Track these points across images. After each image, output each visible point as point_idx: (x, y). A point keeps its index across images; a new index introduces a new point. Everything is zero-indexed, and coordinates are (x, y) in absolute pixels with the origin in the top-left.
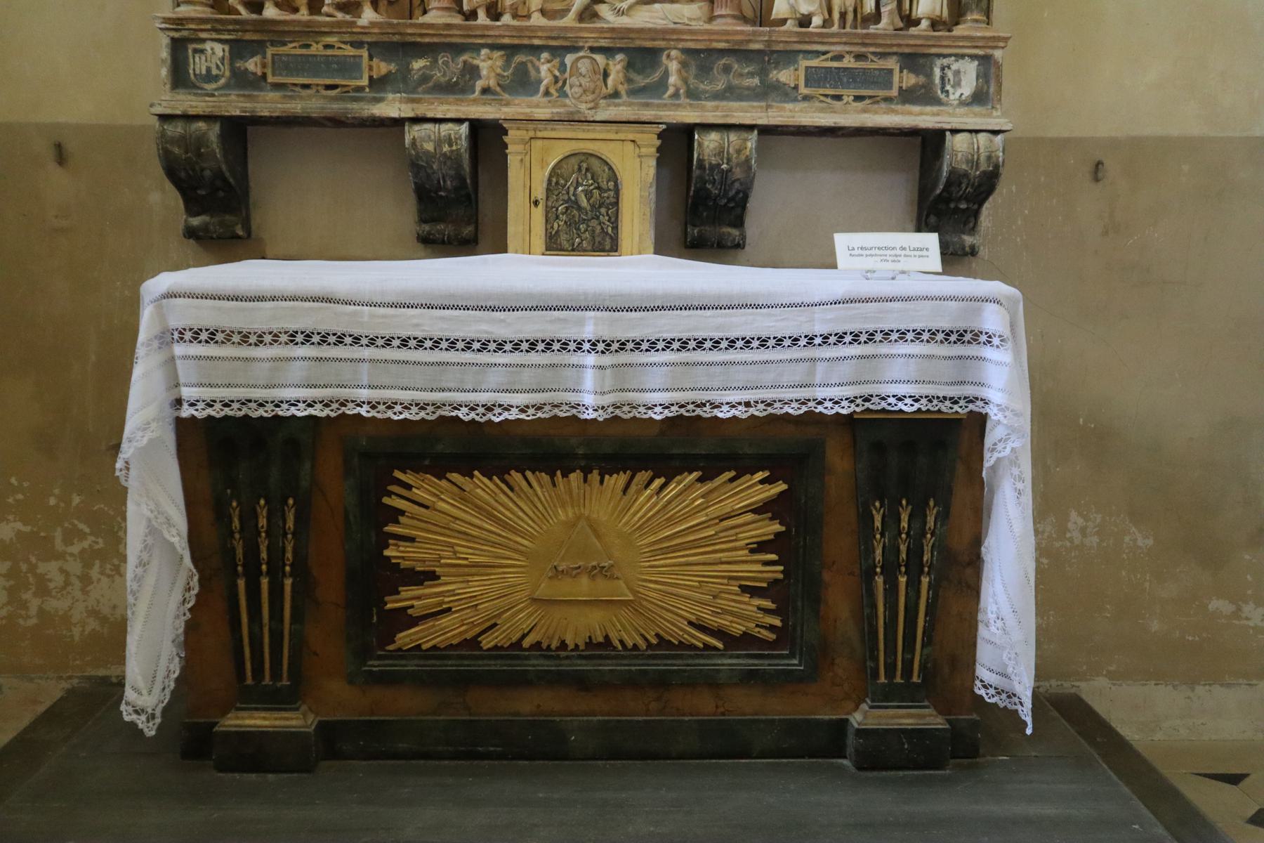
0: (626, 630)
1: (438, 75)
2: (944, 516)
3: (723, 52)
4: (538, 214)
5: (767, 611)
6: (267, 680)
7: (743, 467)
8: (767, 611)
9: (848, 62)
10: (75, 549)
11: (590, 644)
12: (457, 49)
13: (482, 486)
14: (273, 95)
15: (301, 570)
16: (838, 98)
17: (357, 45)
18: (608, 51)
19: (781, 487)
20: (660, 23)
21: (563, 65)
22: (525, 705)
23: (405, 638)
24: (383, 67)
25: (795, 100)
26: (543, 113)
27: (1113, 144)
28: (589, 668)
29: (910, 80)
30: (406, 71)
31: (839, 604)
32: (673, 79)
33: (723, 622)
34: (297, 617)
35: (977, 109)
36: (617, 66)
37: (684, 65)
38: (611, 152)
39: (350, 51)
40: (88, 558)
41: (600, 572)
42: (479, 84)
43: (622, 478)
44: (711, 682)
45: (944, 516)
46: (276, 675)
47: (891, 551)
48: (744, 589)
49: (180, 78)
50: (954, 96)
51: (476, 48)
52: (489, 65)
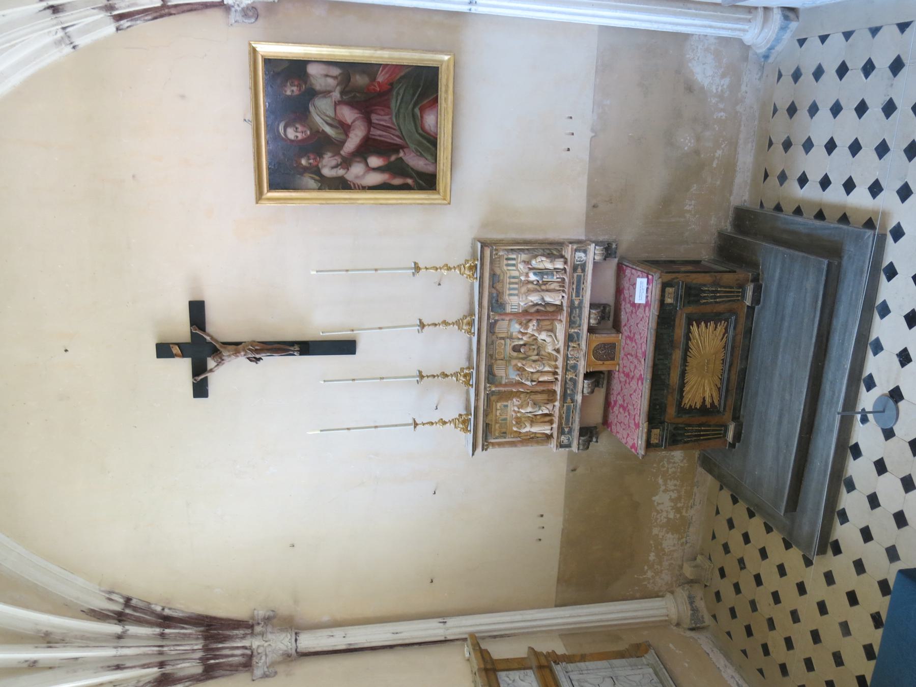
2: (705, 285)
4: (606, 362)
7: (689, 331)
9: (574, 286)
10: (666, 465)
12: (566, 383)
13: (687, 389)
15: (700, 425)
18: (568, 346)
22: (734, 377)
23: (716, 403)
24: (569, 400)
27: (588, 201)
29: (579, 270)
30: (570, 395)
31: (721, 308)
34: (709, 426)
36: (572, 344)
38: (594, 345)
40: (669, 463)
45: (705, 285)
47: (711, 297)
50: (584, 258)
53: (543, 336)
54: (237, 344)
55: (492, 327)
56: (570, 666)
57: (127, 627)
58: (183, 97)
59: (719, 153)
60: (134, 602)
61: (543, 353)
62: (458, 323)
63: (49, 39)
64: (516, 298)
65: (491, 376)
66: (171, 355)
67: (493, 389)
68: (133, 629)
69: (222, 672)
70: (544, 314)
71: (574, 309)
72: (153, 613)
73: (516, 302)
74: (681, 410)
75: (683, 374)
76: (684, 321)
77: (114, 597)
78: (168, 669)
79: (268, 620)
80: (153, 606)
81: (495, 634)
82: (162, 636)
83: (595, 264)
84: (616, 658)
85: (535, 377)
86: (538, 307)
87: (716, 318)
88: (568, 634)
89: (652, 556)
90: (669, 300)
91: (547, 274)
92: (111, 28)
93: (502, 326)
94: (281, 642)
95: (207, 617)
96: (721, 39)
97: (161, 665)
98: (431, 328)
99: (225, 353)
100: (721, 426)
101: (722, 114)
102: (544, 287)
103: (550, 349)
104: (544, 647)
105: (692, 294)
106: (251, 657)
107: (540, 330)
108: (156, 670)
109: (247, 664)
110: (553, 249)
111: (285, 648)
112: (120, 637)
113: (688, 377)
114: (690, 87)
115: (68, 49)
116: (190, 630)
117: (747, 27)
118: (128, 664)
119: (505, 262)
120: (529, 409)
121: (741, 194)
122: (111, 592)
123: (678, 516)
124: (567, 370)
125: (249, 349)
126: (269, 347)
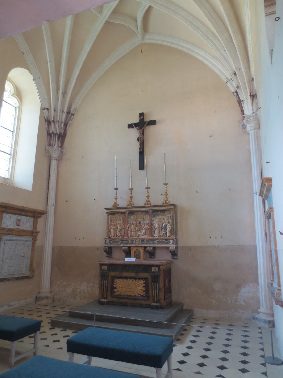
0: (133, 294)
1: (126, 243)
2: (159, 284)
3: (149, 240)
5: (144, 293)
6: (104, 297)
8: (144, 293)
9: (160, 240)
11: (130, 295)
12: (127, 240)
13: (121, 280)
14: (112, 245)
16: (160, 244)
17: (119, 240)
18: (139, 240)
19: (145, 281)
20: (144, 237)
21: (136, 242)
22: (125, 301)
23: (115, 294)
24: (121, 242)
25: (156, 244)
26: (134, 246)
28: (129, 298)
29: (166, 242)
32: (145, 242)
33: (140, 294)
35: (173, 245)
36: (140, 241)
37: (146, 241)
39: (118, 241)
41: (130, 288)
42: (129, 243)
43: (132, 280)
44: (138, 299)
45: (159, 284)
46: (105, 296)
47: (154, 288)
48: (142, 291)
49: (106, 243)
51: (129, 240)
52: (130, 241)
53: (144, 231)
54: (143, 134)
55: (147, 212)
56: (31, 243)
57: (65, 113)
58: (216, 112)
59: (214, 301)
60: (72, 116)
61: (138, 232)
62: (148, 200)
63: (228, 76)
64: (157, 221)
65: (131, 213)
66: (140, 117)
67: (126, 214)
68: (64, 115)
69: (49, 138)
70: (152, 230)
71: (152, 240)
72: (69, 121)
73: (156, 222)
74: (114, 278)
75: (126, 278)
76: (145, 276)
77: (75, 111)
78: (52, 123)
79: (62, 152)
80: (71, 121)
81: (47, 223)
82: (62, 122)
83: (168, 248)
84: (31, 261)
85: (130, 229)
86: (154, 229)
87: (147, 291)
88: (42, 249)
89: (65, 283)
90: (153, 269)
91: (165, 230)
92: (233, 90)
93: (147, 217)
94: (55, 155)
95: (66, 136)
96: (258, 299)
97: (54, 121)
98: (147, 192)
99: (140, 130)
100: (107, 297)
101: (230, 302)
102: (160, 229)
103: (139, 233)
104: (39, 237)
105: (155, 279)
106: (52, 146)
107: (145, 229)
108: (52, 119)
109: (50, 145)
110: (174, 231)
111: (53, 156)
112: (63, 111)
113: (125, 280)
114: (238, 287)
115: (226, 81)
116: (62, 130)
117: (264, 307)
118: (55, 113)
119: (169, 216)
120: (119, 227)
121: (199, 312)
122: (76, 110)
123: (78, 293)
124: (131, 240)
125: (141, 137)
126: (142, 143)
